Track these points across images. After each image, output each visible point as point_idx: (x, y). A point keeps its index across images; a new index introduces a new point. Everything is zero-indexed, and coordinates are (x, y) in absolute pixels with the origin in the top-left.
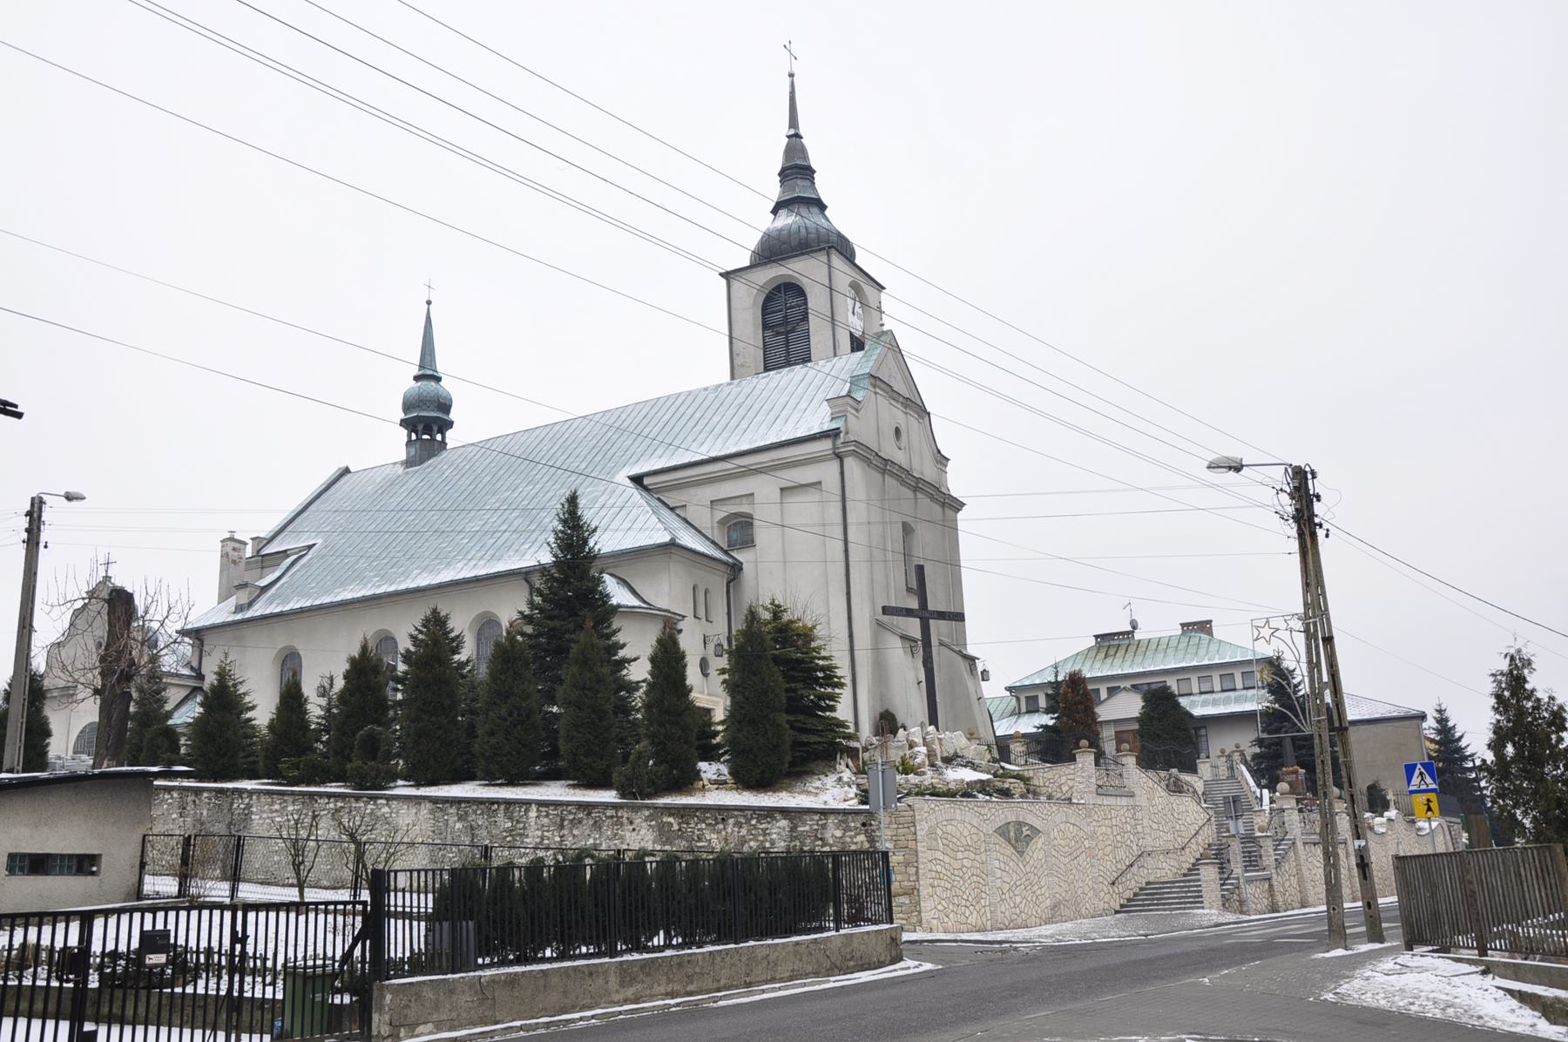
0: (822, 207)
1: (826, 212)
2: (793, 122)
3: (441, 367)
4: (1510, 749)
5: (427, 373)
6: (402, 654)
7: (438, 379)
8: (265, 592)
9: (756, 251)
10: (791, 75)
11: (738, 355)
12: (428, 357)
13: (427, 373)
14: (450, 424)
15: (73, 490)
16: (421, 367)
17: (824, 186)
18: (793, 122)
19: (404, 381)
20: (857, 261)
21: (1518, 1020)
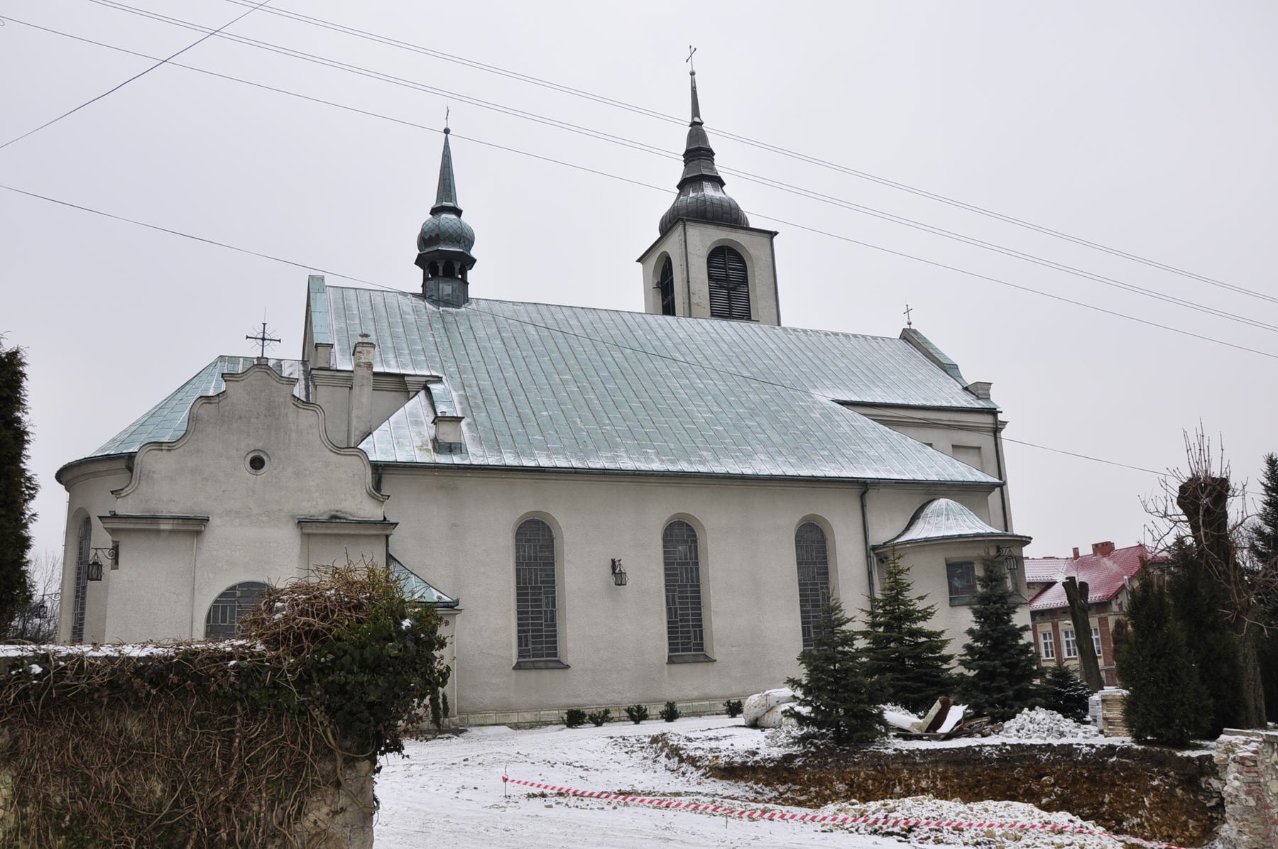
0: (722, 184)
1: (724, 188)
2: (695, 111)
3: (462, 199)
4: (37, 669)
5: (446, 204)
6: (974, 642)
7: (458, 212)
8: (116, 520)
9: (689, 209)
10: (693, 74)
11: (693, 294)
12: (446, 158)
13: (446, 204)
14: (472, 261)
15: (601, 811)
16: (439, 198)
17: (722, 165)
18: (695, 111)
19: (419, 217)
20: (752, 225)
21: (653, 798)
